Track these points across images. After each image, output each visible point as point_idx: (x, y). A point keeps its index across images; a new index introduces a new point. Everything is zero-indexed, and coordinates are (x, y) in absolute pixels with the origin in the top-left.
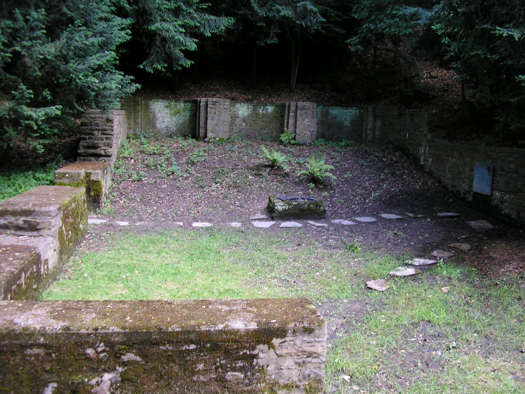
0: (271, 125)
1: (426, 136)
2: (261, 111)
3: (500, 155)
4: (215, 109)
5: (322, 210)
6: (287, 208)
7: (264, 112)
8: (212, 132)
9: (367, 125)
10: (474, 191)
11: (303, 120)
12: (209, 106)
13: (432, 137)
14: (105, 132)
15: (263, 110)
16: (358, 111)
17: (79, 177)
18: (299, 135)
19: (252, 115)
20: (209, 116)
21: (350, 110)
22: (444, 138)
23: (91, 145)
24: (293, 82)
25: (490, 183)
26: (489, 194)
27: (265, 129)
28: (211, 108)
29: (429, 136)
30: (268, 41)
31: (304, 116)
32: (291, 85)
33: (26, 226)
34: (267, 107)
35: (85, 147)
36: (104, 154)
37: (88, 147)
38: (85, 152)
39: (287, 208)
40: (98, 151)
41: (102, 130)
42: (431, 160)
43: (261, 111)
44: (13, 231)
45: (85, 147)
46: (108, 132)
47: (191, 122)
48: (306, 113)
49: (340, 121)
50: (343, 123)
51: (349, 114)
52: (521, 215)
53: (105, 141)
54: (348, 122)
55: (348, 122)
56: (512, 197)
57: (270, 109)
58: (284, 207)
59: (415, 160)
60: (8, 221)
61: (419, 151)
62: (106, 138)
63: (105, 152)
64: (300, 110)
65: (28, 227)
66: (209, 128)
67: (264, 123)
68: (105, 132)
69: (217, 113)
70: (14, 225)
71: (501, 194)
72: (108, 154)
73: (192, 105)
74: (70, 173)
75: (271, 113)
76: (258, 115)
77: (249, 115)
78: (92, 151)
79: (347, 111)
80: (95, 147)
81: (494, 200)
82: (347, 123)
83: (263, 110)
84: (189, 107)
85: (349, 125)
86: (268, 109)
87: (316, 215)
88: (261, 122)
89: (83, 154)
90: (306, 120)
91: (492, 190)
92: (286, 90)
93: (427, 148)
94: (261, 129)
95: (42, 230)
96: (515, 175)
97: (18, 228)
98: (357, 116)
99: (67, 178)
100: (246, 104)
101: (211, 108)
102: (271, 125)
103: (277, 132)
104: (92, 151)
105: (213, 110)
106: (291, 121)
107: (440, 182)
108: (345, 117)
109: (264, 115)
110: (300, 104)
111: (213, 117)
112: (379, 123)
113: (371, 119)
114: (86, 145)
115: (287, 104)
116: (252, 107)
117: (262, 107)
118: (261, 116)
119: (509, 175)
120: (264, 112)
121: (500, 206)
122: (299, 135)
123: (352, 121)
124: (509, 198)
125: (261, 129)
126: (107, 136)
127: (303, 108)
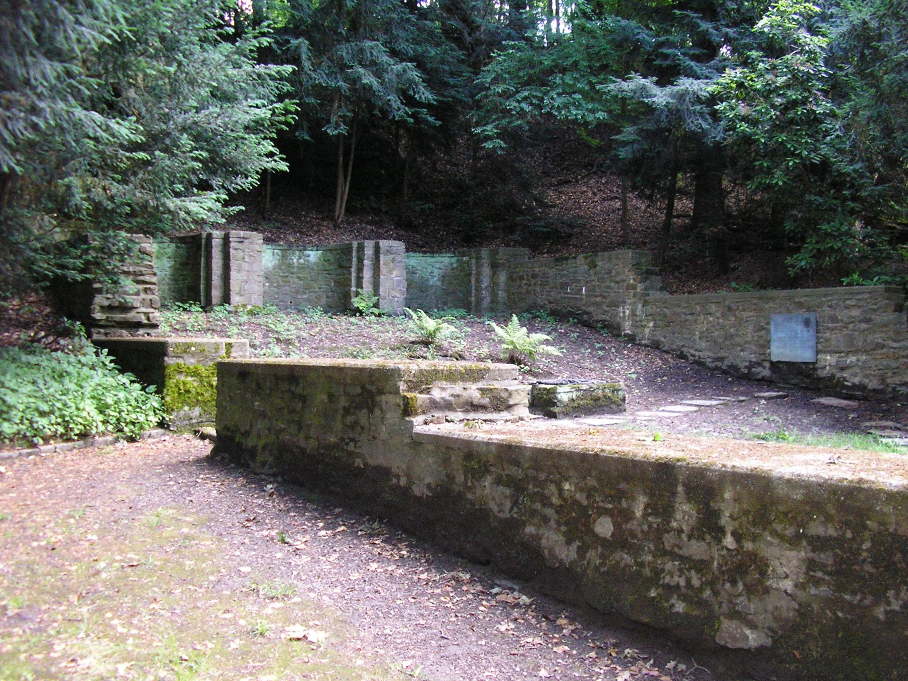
0: (315, 285)
1: (634, 287)
2: (295, 260)
3: (823, 299)
4: (243, 251)
5: (621, 397)
6: (574, 397)
7: (302, 261)
8: (240, 294)
9: (478, 281)
10: (774, 359)
11: (390, 272)
12: (232, 244)
13: (646, 289)
14: (141, 278)
15: (300, 258)
16: (454, 260)
17: (216, 352)
18: (385, 298)
19: (278, 267)
20: (233, 264)
21: (440, 259)
22: (662, 289)
23: (117, 304)
24: (340, 209)
25: (812, 343)
26: (813, 360)
27: (304, 293)
28: (235, 249)
29: (640, 287)
30: (328, 131)
31: (392, 265)
32: (337, 214)
33: (486, 401)
34: (307, 252)
35: (103, 309)
36: (146, 322)
37: (110, 308)
38: (107, 319)
39: (574, 397)
40: (131, 316)
41: (135, 274)
42: (651, 324)
43: (295, 260)
44: (461, 415)
45: (103, 309)
46: (147, 278)
47: (176, 280)
48: (393, 261)
49: (422, 278)
50: (427, 280)
51: (437, 266)
52: (889, 381)
53: (143, 296)
54: (435, 279)
55: (435, 279)
56: (864, 357)
57: (314, 255)
58: (570, 394)
59: (612, 329)
60: (449, 392)
61: (617, 314)
62: (146, 290)
63: (148, 319)
64: (385, 254)
65: (491, 402)
66: (234, 286)
67: (301, 282)
68: (141, 278)
69: (247, 259)
70: (462, 400)
71: (839, 357)
72: (154, 322)
73: (177, 247)
74: (200, 344)
75: (315, 264)
76: (290, 266)
77: (275, 268)
78: (119, 316)
79: (433, 260)
80: (125, 308)
81: (824, 368)
82: (435, 281)
83: (300, 258)
84: (169, 250)
85: (439, 283)
86: (309, 256)
87: (613, 406)
88: (297, 280)
89: (102, 323)
90: (395, 272)
91: (818, 352)
92: (325, 223)
93: (640, 306)
94: (297, 292)
95: (516, 408)
96: (864, 326)
97: (473, 407)
98: (453, 269)
99: (193, 355)
100: (269, 247)
101: (235, 249)
102: (315, 285)
103: (328, 297)
104: (119, 316)
105: (240, 254)
106: (367, 274)
107: (682, 356)
108: (430, 269)
109: (301, 268)
110: (383, 244)
111: (240, 265)
112: (502, 278)
113: (486, 271)
114: (106, 303)
115: (355, 244)
116: (279, 252)
117: (297, 253)
118: (295, 270)
119: (851, 326)
120: (302, 261)
121: (839, 375)
122: (385, 298)
123: (443, 278)
124: (858, 360)
125: (297, 292)
126: (148, 286)
127: (389, 252)
